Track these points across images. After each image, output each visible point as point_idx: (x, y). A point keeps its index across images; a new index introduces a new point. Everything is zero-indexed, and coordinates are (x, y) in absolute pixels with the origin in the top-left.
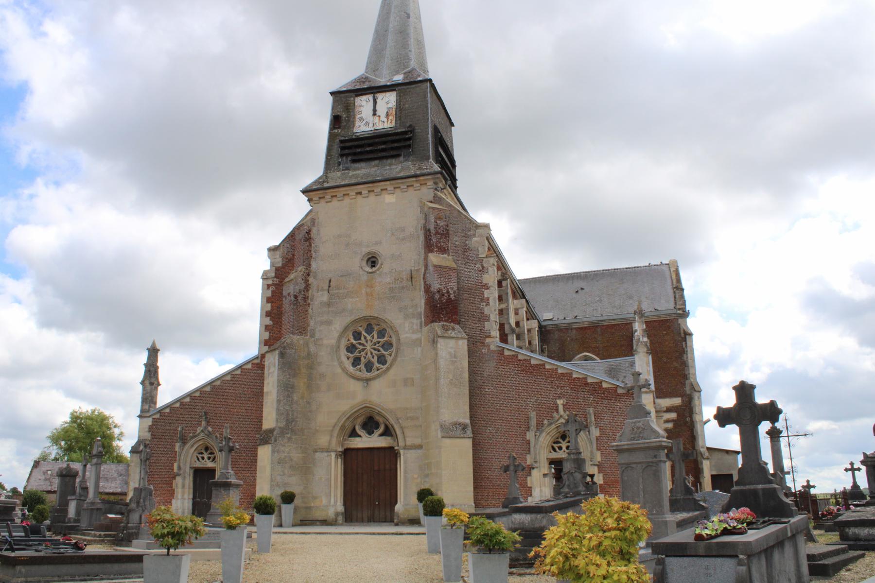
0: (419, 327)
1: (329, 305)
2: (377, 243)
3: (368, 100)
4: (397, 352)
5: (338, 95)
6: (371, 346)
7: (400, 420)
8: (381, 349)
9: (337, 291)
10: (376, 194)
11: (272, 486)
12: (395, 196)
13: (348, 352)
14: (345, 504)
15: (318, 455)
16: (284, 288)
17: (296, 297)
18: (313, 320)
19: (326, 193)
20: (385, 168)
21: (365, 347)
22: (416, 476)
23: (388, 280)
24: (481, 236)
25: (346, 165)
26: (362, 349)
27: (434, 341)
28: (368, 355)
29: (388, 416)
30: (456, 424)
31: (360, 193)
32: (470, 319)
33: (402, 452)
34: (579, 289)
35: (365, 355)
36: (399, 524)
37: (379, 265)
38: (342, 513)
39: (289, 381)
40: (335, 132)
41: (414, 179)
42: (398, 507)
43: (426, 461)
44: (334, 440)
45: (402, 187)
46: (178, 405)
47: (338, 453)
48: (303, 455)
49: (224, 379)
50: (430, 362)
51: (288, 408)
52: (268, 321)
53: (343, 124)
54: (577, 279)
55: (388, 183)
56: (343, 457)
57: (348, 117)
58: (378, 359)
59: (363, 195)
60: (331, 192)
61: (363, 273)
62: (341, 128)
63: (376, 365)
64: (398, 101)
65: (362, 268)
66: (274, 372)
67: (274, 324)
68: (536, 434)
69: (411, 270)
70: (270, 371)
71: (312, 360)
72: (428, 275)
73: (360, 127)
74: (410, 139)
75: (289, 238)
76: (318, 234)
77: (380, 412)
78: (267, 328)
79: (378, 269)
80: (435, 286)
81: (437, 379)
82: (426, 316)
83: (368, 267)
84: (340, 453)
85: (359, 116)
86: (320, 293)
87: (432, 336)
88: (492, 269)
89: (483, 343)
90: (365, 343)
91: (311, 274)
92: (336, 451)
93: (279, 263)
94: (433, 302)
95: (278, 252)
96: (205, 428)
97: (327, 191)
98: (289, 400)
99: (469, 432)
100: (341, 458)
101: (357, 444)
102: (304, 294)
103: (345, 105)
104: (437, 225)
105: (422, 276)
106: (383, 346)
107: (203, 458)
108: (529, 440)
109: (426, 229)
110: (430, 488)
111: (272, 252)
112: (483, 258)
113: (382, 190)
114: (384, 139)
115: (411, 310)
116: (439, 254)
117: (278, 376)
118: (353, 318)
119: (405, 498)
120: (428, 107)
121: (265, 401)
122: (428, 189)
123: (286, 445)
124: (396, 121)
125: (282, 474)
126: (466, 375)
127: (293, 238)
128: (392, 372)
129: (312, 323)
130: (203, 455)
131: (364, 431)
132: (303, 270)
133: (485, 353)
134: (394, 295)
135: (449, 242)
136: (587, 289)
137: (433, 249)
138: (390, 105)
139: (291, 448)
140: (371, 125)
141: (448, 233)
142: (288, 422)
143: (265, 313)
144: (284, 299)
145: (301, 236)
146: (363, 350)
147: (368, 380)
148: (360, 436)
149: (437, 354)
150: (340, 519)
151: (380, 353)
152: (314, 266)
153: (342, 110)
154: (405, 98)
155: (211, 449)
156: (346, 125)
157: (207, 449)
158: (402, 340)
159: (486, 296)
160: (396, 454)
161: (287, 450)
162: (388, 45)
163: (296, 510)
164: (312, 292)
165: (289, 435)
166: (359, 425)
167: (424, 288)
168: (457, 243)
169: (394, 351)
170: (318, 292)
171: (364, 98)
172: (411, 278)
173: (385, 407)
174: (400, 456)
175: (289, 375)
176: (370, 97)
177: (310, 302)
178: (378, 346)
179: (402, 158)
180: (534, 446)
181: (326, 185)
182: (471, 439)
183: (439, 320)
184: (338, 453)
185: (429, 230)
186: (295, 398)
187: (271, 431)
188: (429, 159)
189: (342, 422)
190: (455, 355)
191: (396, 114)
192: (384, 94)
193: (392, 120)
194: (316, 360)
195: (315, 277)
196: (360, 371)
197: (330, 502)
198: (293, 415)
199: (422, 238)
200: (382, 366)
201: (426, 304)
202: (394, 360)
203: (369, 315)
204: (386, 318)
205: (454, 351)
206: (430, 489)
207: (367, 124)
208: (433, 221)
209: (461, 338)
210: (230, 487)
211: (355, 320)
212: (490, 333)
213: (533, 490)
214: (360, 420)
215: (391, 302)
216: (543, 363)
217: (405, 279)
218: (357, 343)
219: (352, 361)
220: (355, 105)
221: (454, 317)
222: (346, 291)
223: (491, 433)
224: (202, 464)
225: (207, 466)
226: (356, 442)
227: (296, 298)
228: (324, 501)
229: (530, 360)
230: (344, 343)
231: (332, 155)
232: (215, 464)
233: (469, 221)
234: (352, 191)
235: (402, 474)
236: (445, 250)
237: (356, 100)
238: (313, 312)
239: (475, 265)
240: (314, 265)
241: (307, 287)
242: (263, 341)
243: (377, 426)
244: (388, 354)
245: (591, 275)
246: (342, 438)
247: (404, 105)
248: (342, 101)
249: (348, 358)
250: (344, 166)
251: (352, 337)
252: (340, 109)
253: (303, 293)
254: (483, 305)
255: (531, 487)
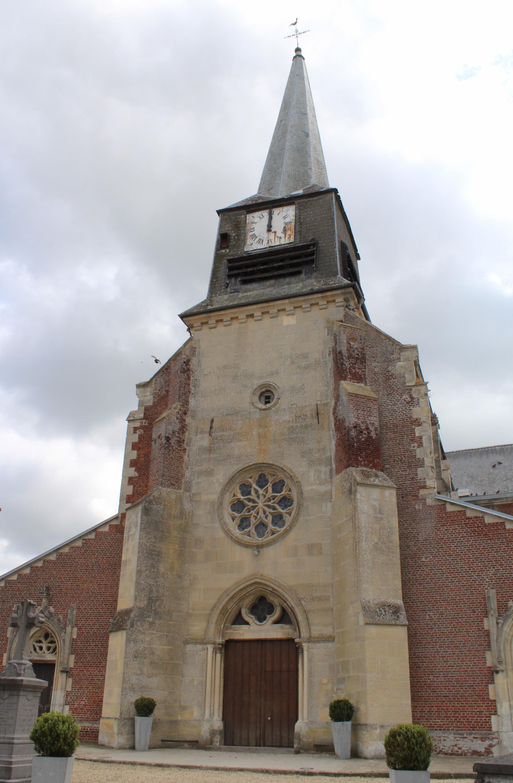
0: (328, 476)
1: (210, 450)
2: (272, 374)
3: (261, 216)
4: (299, 508)
5: (227, 213)
6: (264, 502)
7: (303, 602)
8: (277, 506)
9: (220, 433)
10: (271, 315)
11: (123, 689)
12: (295, 317)
13: (233, 511)
14: (224, 718)
15: (189, 648)
16: (154, 429)
17: (168, 439)
18: (190, 469)
19: (210, 316)
20: (283, 287)
21: (256, 504)
22: (325, 681)
23: (287, 418)
24: (407, 360)
25: (235, 287)
26: (252, 507)
27: (350, 491)
28: (260, 513)
29: (287, 596)
30: (384, 606)
31: (252, 316)
32: (398, 464)
33: (305, 646)
34: (496, 463)
35: (256, 515)
36: (301, 751)
37: (275, 400)
38: (220, 731)
39: (154, 546)
40: (222, 253)
41: (320, 295)
42: (300, 726)
43: (341, 660)
44: (212, 627)
45: (304, 306)
46: (15, 577)
47: (217, 646)
48: (170, 647)
49: (73, 545)
50: (345, 520)
51: (151, 581)
52: (132, 472)
53: (231, 244)
54: (493, 453)
55: (287, 301)
56: (223, 651)
57: (237, 236)
58: (273, 520)
59: (255, 318)
60: (218, 315)
61: (255, 410)
62: (230, 247)
63: (271, 526)
64: (298, 215)
65: (253, 404)
66: (135, 534)
67: (140, 476)
68: (498, 621)
69: (317, 405)
70: (131, 533)
71: (186, 520)
72: (340, 408)
73: (252, 244)
74: (312, 254)
75: (163, 371)
76: (199, 365)
77: (275, 590)
78: (130, 481)
79: (274, 405)
80: (351, 420)
81: (356, 543)
82: (339, 461)
83: (261, 403)
84: (220, 646)
85: (251, 234)
86: (200, 436)
87: (349, 485)
88: (425, 400)
89: (417, 496)
90: (256, 499)
91: (189, 413)
92: (214, 643)
93: (149, 400)
94: (348, 440)
95: (149, 389)
96: (46, 608)
97: (212, 314)
98: (154, 572)
99: (403, 618)
100: (221, 653)
101: (243, 634)
102: (178, 437)
103: (234, 223)
104: (351, 347)
105: (331, 411)
106: (279, 503)
107: (41, 648)
108: (488, 630)
109: (336, 352)
110: (347, 698)
111: (142, 389)
112: (412, 386)
113: (279, 311)
114: (281, 255)
115: (317, 455)
116: (353, 382)
117: (140, 539)
118: (240, 466)
119: (309, 712)
120: (334, 218)
121: (121, 573)
122: (337, 307)
123: (147, 632)
124: (295, 236)
125: (139, 672)
126: (396, 537)
127: (168, 371)
128: (292, 535)
129: (188, 474)
130: (41, 644)
131: (253, 616)
132: (179, 406)
133: (419, 510)
134: (295, 436)
135: (365, 368)
136: (505, 463)
137: (346, 376)
138: (288, 220)
139: (153, 637)
140: (265, 242)
141: (364, 358)
142: (150, 601)
143: (129, 463)
144: (153, 443)
145: (177, 368)
146: (254, 507)
147: (259, 547)
148: (247, 623)
149: (355, 508)
150: (217, 740)
151: (276, 511)
152: (192, 403)
153: (230, 229)
154: (306, 211)
155: (52, 637)
156: (235, 244)
157: (47, 636)
158: (305, 494)
159: (417, 435)
160: (297, 649)
161: (147, 639)
162: (284, 162)
163: (155, 725)
164: (189, 434)
165: (151, 620)
166: (246, 608)
167: (335, 425)
168: (376, 370)
169: (295, 508)
170: (197, 435)
171: (257, 214)
172: (318, 414)
173: (282, 583)
174: (302, 652)
175: (155, 537)
176: (265, 213)
177: (185, 447)
178: (273, 503)
179: (303, 276)
180: (497, 639)
181: (210, 307)
182: (406, 628)
183: (357, 464)
184: (217, 646)
185: (340, 352)
186: (162, 570)
187: (127, 612)
188: (337, 274)
189: (223, 603)
190: (380, 510)
191: (295, 229)
192: (280, 209)
193: (290, 235)
194: (192, 521)
195: (192, 417)
196: (249, 536)
197: (204, 714)
198: (157, 591)
199: (330, 364)
200: (279, 529)
201: (338, 445)
202: (295, 520)
203: (263, 462)
204: (284, 466)
205: (379, 504)
206: (348, 701)
207: (261, 241)
208: (345, 341)
209: (388, 487)
210: (20, 690)
211: (244, 469)
212: (425, 482)
213: (498, 706)
214: (248, 601)
215: (291, 445)
216: (502, 521)
217: (309, 416)
218: (245, 499)
219: (239, 523)
220: (246, 223)
221: (376, 461)
222: (232, 433)
223: (431, 619)
224: (38, 656)
225: (45, 659)
226: (241, 632)
227: (168, 441)
228: (196, 714)
229: (483, 517)
230: (228, 498)
231: (219, 277)
232: (55, 656)
233: (391, 343)
234: (240, 314)
235: (306, 677)
236: (361, 378)
237: (248, 218)
238: (189, 460)
239: (401, 396)
240: (192, 402)
241: (183, 428)
242: (125, 497)
243: (271, 609)
244: (286, 513)
245: (507, 449)
246: (222, 626)
247: (304, 219)
248: (231, 219)
249: (233, 519)
250: (232, 288)
251: (239, 491)
252: (228, 229)
253: (177, 435)
254: (414, 447)
255: (495, 701)
